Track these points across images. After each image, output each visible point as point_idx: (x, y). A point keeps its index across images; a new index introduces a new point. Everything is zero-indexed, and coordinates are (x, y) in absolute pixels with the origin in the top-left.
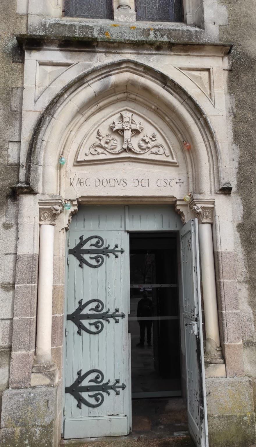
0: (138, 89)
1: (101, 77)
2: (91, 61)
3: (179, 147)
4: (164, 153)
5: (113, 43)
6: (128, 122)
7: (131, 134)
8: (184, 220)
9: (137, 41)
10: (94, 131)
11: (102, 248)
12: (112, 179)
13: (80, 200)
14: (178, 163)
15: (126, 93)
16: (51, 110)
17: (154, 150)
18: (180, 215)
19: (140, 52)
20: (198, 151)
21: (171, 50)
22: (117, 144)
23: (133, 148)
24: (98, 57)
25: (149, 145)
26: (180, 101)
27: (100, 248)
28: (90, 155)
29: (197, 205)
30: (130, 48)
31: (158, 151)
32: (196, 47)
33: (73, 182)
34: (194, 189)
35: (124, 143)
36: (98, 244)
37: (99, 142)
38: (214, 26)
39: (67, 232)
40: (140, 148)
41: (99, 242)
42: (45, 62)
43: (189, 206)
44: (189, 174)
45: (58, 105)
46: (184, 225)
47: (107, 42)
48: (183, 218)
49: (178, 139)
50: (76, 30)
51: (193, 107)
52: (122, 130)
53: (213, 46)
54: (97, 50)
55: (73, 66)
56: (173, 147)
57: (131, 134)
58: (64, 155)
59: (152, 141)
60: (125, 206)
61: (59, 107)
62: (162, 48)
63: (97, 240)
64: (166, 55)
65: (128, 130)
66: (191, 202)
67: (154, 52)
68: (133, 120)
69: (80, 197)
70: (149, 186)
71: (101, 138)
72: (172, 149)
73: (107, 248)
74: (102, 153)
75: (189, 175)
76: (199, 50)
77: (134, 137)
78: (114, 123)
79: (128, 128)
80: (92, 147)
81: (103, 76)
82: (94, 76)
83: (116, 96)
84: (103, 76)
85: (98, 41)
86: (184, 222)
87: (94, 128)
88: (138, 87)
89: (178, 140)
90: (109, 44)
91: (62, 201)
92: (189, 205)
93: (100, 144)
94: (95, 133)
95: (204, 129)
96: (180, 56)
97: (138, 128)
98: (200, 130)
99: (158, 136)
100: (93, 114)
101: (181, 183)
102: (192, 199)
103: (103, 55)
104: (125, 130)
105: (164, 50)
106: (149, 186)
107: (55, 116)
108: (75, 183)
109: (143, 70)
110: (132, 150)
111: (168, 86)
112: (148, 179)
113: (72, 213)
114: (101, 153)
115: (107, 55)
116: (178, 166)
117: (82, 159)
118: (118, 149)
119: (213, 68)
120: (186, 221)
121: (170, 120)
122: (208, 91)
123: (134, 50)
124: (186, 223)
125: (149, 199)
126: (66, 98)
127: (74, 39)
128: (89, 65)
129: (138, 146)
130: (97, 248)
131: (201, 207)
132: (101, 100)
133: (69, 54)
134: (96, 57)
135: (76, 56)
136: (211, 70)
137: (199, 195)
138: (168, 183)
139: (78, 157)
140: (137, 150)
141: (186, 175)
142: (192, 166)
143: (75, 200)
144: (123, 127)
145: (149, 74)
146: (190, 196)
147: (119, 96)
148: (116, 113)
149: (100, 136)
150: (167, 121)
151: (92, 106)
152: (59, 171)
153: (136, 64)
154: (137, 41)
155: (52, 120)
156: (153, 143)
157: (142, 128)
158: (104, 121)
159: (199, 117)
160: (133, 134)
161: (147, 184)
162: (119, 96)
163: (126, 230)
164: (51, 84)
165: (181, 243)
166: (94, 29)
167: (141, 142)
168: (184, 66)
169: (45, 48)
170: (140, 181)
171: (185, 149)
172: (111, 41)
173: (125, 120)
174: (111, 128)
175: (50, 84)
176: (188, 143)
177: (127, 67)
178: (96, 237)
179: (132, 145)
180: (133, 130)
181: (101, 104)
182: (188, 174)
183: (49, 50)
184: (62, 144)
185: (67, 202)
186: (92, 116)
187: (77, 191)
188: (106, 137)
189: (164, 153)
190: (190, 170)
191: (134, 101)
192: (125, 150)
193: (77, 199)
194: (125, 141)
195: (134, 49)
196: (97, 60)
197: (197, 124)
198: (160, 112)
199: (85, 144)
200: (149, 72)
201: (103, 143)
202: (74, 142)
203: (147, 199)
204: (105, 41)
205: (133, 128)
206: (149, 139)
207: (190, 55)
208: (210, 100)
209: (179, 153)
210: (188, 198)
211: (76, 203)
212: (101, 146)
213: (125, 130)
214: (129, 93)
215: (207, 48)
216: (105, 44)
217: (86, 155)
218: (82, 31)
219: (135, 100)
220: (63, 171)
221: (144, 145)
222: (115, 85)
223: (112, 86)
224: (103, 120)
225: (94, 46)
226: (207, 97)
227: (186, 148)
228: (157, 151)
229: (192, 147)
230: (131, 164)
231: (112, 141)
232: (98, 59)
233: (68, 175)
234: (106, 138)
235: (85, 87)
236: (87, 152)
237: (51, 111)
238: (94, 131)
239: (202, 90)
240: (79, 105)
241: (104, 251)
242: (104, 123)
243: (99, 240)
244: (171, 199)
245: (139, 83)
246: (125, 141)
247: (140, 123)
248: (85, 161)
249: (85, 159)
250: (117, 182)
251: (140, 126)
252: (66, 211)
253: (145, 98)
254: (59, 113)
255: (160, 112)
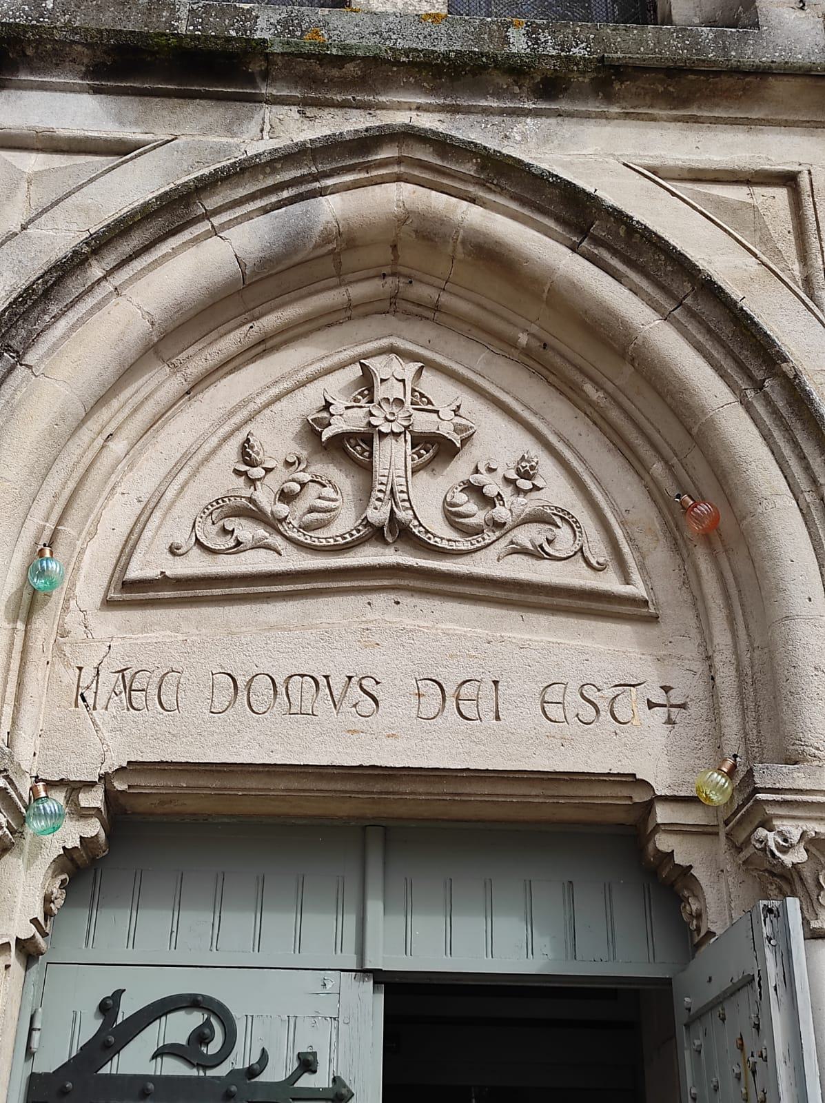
0: (453, 258)
1: (274, 199)
2: (233, 135)
3: (657, 525)
4: (581, 549)
5: (339, 61)
6: (399, 402)
7: (409, 459)
8: (699, 916)
9: (452, 55)
10: (225, 439)
11: (222, 1071)
12: (302, 676)
13: (120, 786)
14: (655, 604)
15: (389, 280)
16: (14, 325)
17: (527, 536)
18: (672, 885)
19: (463, 102)
20: (766, 537)
21: (609, 98)
22: (337, 504)
23: (421, 525)
24: (267, 121)
25: (501, 513)
26: (656, 307)
27: (210, 1073)
28: (196, 551)
29: (776, 822)
30: (418, 87)
31: (549, 542)
32: (726, 82)
33: (94, 685)
34: (753, 736)
35: (373, 500)
36: (204, 1049)
37: (247, 492)
38: (802, 14)
39: (34, 968)
40: (454, 526)
41: (207, 1031)
42: (17, 135)
43: (728, 835)
44: (718, 658)
45: (54, 309)
46: (698, 946)
47: (309, 56)
48: (695, 906)
49: (651, 485)
50: (179, 19)
51: (727, 331)
52: (367, 437)
53: (808, 81)
54: (264, 92)
55: (145, 152)
56: (623, 524)
57: (409, 459)
58: (61, 548)
59: (518, 491)
60: (364, 828)
61: (56, 318)
62: (566, 89)
63: (196, 1019)
64: (587, 116)
65: (396, 435)
66: (735, 814)
67: (529, 105)
68: (422, 395)
69: (122, 769)
70: (498, 718)
71: (257, 472)
72: (619, 533)
73: (252, 1072)
74: (259, 547)
75: (718, 665)
76: (739, 98)
77: (422, 475)
78: (327, 406)
79: (396, 430)
80: (211, 513)
81: (285, 194)
82: (241, 192)
83: (342, 290)
84: (285, 194)
85: (273, 54)
86: (698, 929)
87: (226, 428)
88: (450, 249)
89: (654, 492)
90: (321, 66)
91: (11, 782)
92: (723, 831)
93: (251, 500)
94: (231, 450)
95: (787, 429)
96: (653, 123)
97: (446, 430)
98: (767, 437)
99: (548, 470)
100: (229, 365)
101: (672, 706)
102: (746, 786)
103: (293, 111)
104: (383, 435)
105: (573, 98)
106: (498, 718)
107: (31, 358)
108: (104, 692)
109: (477, 171)
110: (416, 531)
111: (598, 242)
112: (496, 683)
113: (72, 860)
114: (249, 546)
115: (310, 112)
116: (654, 619)
117: (152, 573)
118: (344, 524)
119: (810, 173)
120: (715, 921)
121: (608, 395)
122: (796, 267)
123: (437, 96)
124: (710, 934)
125: (502, 789)
126: (99, 281)
127: (163, 41)
128: (224, 150)
129: (447, 518)
130: (194, 1072)
131: (803, 834)
132: (272, 303)
133: (130, 106)
134: (257, 118)
135: (165, 113)
136: (804, 180)
137: (786, 769)
138: (603, 706)
139: (133, 559)
140: (441, 532)
141: (699, 666)
142: (731, 620)
143: (90, 785)
144: (369, 424)
145: (502, 189)
146: (731, 774)
147: (359, 291)
148: (342, 366)
149: (253, 465)
150: (590, 403)
151: (222, 330)
152: (20, 626)
153: (442, 144)
154: (452, 55)
155: (15, 373)
156: (521, 499)
157: (467, 428)
158: (278, 398)
159: (759, 374)
160: (420, 456)
161: (487, 705)
162: (359, 291)
163: (368, 966)
164: (32, 221)
165: (687, 1057)
166: (257, 17)
167: (462, 498)
168: (672, 163)
169: (24, 77)
170: (450, 690)
171: (688, 534)
172: (331, 55)
173: (380, 392)
174: (313, 429)
175: (28, 224)
176: (704, 501)
177: (399, 161)
178: (193, 1002)
179: (412, 508)
180: (420, 441)
181: (270, 321)
182: (709, 658)
183: (43, 87)
184: (56, 496)
185: (43, 794)
186: (221, 372)
187: (106, 735)
188: (284, 470)
189: (581, 549)
190: (721, 637)
191: (430, 314)
192: (375, 534)
193: (104, 778)
194: (380, 491)
195: (433, 91)
196: (262, 131)
197: (748, 407)
198: (558, 361)
199: (173, 502)
200: (503, 182)
201: (265, 498)
202: (119, 490)
203: (486, 789)
204: (301, 55)
205: (417, 428)
206: (500, 481)
207: (696, 120)
208: (811, 304)
209: (660, 555)
210: (717, 787)
211: (93, 799)
212: (253, 513)
213: (383, 435)
214: (405, 276)
215: (780, 87)
216: (301, 67)
217: (174, 551)
218: (201, 24)
219: (436, 308)
220: (43, 626)
221: (477, 515)
222: (340, 233)
223: (326, 238)
224: (274, 391)
225: (252, 73)
226: (790, 288)
227: (692, 529)
228: (541, 540)
229: (726, 522)
230: (407, 601)
231: (313, 490)
232: (267, 127)
233: (67, 649)
234: (281, 474)
235: (196, 240)
236: (182, 538)
237: (13, 332)
238: (225, 439)
239: (765, 259)
240: (157, 316)
241: (234, 1088)
242: (277, 407)
243: (207, 1023)
244: (625, 792)
245: (458, 227)
246: (380, 491)
247: (459, 407)
248: (165, 582)
249: (168, 573)
250: (327, 690)
251: (457, 420)
252: (38, 846)
253: (484, 301)
254: (56, 345)
255: (558, 361)
